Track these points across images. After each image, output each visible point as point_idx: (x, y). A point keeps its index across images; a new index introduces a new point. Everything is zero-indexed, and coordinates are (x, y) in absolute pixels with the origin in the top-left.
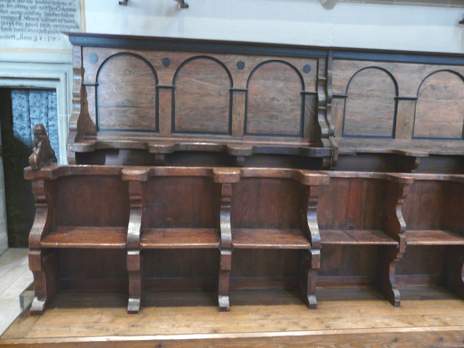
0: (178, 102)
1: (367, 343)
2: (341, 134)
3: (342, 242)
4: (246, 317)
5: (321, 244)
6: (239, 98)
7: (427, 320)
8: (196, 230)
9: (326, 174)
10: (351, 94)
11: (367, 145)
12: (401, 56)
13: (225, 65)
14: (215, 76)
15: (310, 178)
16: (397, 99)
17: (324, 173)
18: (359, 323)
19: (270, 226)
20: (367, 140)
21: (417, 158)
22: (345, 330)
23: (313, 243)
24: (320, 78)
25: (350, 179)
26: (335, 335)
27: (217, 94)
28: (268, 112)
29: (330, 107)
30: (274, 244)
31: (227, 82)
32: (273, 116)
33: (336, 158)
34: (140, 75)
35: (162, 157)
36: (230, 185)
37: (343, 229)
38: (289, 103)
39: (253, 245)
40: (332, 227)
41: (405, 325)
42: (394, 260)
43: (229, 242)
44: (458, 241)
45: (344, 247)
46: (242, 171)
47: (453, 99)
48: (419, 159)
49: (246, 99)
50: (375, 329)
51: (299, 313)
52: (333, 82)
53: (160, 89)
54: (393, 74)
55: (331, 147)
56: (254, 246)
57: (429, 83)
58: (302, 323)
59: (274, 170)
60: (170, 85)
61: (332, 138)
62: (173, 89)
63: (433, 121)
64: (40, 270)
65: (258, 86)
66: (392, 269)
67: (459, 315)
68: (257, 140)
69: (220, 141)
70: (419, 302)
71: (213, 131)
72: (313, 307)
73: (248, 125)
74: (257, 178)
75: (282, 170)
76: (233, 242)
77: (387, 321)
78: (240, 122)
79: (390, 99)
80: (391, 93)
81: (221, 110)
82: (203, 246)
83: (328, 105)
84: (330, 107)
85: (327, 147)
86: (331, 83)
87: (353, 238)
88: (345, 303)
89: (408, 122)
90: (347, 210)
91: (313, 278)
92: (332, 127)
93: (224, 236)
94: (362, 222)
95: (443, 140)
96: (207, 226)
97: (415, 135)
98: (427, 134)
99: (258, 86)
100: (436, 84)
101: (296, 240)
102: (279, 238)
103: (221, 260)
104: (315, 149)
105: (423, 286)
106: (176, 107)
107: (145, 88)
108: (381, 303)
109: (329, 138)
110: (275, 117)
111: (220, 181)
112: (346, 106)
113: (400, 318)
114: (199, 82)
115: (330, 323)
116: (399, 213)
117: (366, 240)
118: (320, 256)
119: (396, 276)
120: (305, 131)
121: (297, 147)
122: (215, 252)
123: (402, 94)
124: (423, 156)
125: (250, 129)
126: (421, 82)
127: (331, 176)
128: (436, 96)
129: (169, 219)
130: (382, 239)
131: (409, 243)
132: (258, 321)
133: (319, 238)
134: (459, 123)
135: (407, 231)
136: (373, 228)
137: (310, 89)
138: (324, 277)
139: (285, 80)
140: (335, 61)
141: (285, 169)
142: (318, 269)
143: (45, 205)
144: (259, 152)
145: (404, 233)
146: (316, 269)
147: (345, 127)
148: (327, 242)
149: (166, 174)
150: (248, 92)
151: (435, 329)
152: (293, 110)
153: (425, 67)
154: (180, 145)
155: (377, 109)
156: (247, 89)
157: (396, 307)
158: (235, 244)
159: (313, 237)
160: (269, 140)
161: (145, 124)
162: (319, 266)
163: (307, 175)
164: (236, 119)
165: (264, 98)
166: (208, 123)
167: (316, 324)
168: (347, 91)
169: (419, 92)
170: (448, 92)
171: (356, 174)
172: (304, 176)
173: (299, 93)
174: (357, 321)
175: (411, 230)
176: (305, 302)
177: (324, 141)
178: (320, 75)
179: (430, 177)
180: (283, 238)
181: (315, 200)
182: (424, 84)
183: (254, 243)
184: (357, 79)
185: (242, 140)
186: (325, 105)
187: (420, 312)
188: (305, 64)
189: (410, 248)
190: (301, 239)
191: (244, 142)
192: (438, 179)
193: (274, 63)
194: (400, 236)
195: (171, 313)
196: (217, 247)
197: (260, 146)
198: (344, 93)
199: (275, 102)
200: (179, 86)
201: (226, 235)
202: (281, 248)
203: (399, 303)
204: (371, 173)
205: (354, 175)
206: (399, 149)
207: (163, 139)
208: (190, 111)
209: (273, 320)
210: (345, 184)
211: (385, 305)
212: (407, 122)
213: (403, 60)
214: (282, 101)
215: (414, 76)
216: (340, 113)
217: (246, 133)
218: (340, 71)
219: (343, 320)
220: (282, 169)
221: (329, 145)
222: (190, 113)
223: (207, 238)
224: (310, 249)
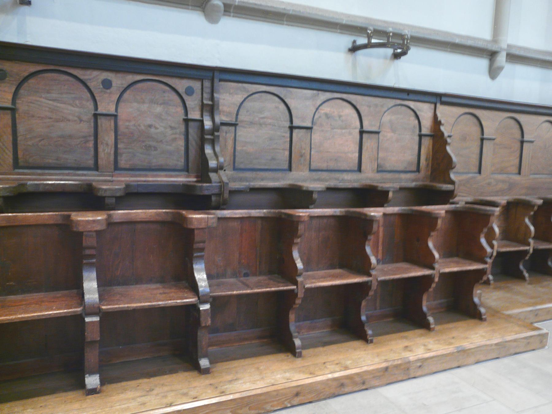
0: (21, 129)
1: (267, 403)
3: (235, 292)
4: (122, 396)
5: (211, 297)
6: (105, 124)
7: (328, 367)
8: (52, 294)
9: (214, 214)
10: (242, 121)
11: (262, 180)
12: (293, 81)
13: (86, 82)
14: (73, 96)
16: (292, 128)
17: (211, 213)
18: (258, 382)
19: (150, 281)
21: (314, 193)
22: (242, 393)
24: (205, 102)
25: (241, 219)
26: (231, 400)
27: (76, 118)
28: (143, 142)
29: (218, 136)
30: (154, 302)
32: (150, 146)
33: (226, 195)
36: (94, 234)
37: (237, 277)
38: (169, 132)
39: (126, 306)
40: (224, 275)
41: (307, 376)
42: (292, 307)
43: (95, 306)
44: (355, 278)
45: (239, 296)
46: (110, 216)
49: (115, 126)
50: (274, 386)
51: (189, 382)
52: (220, 108)
54: (286, 100)
55: (220, 182)
56: (128, 307)
57: (323, 112)
58: (193, 393)
59: (151, 212)
60: (9, 105)
61: (221, 172)
65: (130, 110)
66: (292, 317)
67: (359, 356)
68: (132, 177)
69: (83, 178)
70: (321, 349)
72: (206, 372)
73: (119, 158)
74: (131, 223)
75: (161, 212)
76: (101, 305)
77: (287, 375)
78: (109, 154)
79: (284, 127)
81: (83, 139)
83: (216, 134)
84: (218, 136)
85: (215, 182)
86: (218, 108)
87: (248, 286)
88: (242, 362)
89: (304, 153)
90: (240, 254)
91: (203, 337)
92: (221, 159)
93: (88, 299)
94: (258, 267)
97: (312, 167)
98: (324, 166)
99: (130, 110)
101: (181, 294)
102: (160, 294)
103: (86, 329)
105: (325, 330)
108: (282, 356)
109: (218, 173)
110: (153, 149)
111: (81, 229)
112: (237, 135)
113: (301, 370)
114: (50, 102)
115: (226, 387)
116: (296, 254)
117: (261, 287)
118: (210, 311)
119: (298, 324)
121: (181, 184)
122: (78, 319)
123: (296, 123)
124: (320, 189)
125: (122, 163)
126: (316, 109)
127: (220, 216)
128: (331, 125)
130: (279, 284)
131: (379, 279)
132: (139, 400)
133: (208, 290)
135: (304, 273)
136: (270, 272)
137: (195, 115)
138: (218, 334)
139: (165, 103)
140: (222, 83)
141: (164, 211)
142: (209, 326)
144: (136, 191)
145: (301, 276)
146: (206, 327)
147: (237, 159)
148: (217, 294)
150: (119, 118)
151: (336, 375)
152: (175, 140)
153: (319, 94)
154: (27, 184)
155: (271, 139)
156: (116, 113)
157: (298, 357)
158: (104, 307)
159: (201, 289)
160: (146, 176)
162: (209, 322)
163: (190, 216)
164: (104, 150)
165: (139, 125)
167: (209, 391)
168: (237, 118)
170: (342, 121)
171: (248, 213)
172: (187, 218)
173: (181, 119)
174: (255, 381)
175: (311, 271)
176: (196, 367)
177: (213, 176)
179: (326, 212)
180: (165, 293)
181: (201, 245)
182: (319, 112)
183: (127, 303)
185: (112, 177)
186: (212, 134)
187: (321, 359)
189: (443, 275)
190: (187, 293)
191: (114, 179)
192: (335, 214)
193: (149, 83)
195: (16, 410)
196: (79, 313)
197: (136, 183)
198: (234, 120)
199: (153, 130)
200: (22, 106)
201: (91, 296)
202: (162, 306)
204: (265, 211)
206: (296, 183)
208: (40, 141)
209: (157, 395)
210: (236, 224)
211: (286, 358)
214: (161, 129)
215: (308, 103)
217: (117, 168)
218: (228, 94)
219: (240, 382)
220: (161, 211)
221: (218, 180)
222: (40, 144)
223: (66, 302)
224: (197, 303)
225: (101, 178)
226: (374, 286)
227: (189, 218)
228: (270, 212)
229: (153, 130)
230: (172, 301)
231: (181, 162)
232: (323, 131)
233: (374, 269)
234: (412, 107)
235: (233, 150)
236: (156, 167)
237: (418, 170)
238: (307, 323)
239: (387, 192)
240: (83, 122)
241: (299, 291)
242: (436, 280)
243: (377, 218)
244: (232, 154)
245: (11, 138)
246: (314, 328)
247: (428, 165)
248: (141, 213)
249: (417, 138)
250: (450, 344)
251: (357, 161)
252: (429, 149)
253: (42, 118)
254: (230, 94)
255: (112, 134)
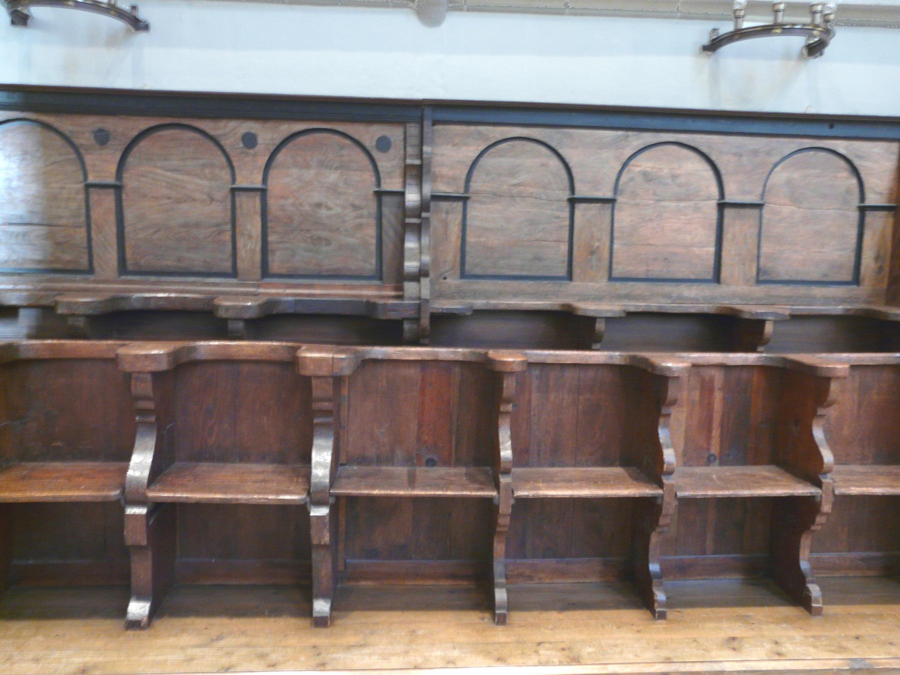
2: (458, 272)
6: (250, 205)
10: (477, 193)
14: (201, 162)
15: (308, 361)
16: (573, 202)
19: (262, 458)
20: (514, 284)
21: (598, 320)
23: (312, 492)
25: (422, 364)
27: (205, 197)
28: (308, 231)
29: (427, 219)
31: (226, 175)
32: (319, 238)
34: (53, 163)
35: (81, 323)
38: (350, 214)
43: (140, 490)
47: (690, 200)
48: (603, 320)
53: (91, 190)
54: (561, 151)
56: (187, 498)
57: (638, 169)
59: (263, 346)
62: (118, 189)
63: (652, 245)
64: (145, 543)
71: (202, 270)
72: (321, 623)
73: (270, 258)
78: (253, 251)
79: (559, 200)
80: (560, 190)
81: (215, 229)
82: (85, 496)
83: (424, 215)
85: (411, 298)
86: (429, 171)
89: (598, 247)
90: (420, 425)
94: (454, 451)
95: (675, 284)
96: (280, 459)
97: (615, 274)
98: (640, 270)
99: (288, 180)
100: (654, 170)
104: (385, 304)
106: (126, 224)
107: (63, 188)
112: (468, 216)
114: (169, 174)
116: (818, 434)
118: (327, 520)
120: (385, 269)
121: (364, 300)
123: (582, 191)
124: (609, 315)
125: (276, 263)
128: (655, 194)
129: (59, 444)
134: (706, 249)
135: (514, 470)
137: (392, 184)
139: (342, 167)
140: (438, 127)
143: (330, 420)
144: (291, 311)
149: (46, 355)
150: (269, 194)
152: (360, 227)
154: (131, 298)
155: (532, 222)
161: (67, 257)
164: (245, 246)
165: (301, 204)
166: (190, 255)
169: (620, 187)
170: (680, 185)
176: (307, 612)
178: (411, 155)
179: (591, 357)
184: (486, 161)
186: (419, 216)
188: (379, 136)
189: (523, 504)
193: (318, 135)
194: (823, 480)
196: (114, 499)
198: (462, 190)
199: (323, 212)
200: (130, 181)
203: (504, 616)
205: (428, 353)
207: (101, 286)
208: (156, 232)
212: (595, 247)
213: (515, 122)
214: (337, 210)
215: (605, 154)
216: (455, 230)
217: (265, 272)
222: (155, 237)
225: (241, 289)
226: (670, 507)
227: (301, 357)
228: (474, 353)
229: (323, 212)
230: (261, 496)
231: (371, 264)
232: (637, 205)
233: (670, 473)
234: (842, 151)
235: (459, 242)
236: (330, 273)
237: (856, 280)
238: (551, 562)
239: (762, 323)
240: (214, 203)
241: (501, 501)
242: (826, 508)
243: (674, 372)
244: (458, 250)
245: (114, 229)
246: (563, 574)
247: (881, 269)
248: (247, 346)
249: (854, 215)
250: (842, 649)
251: (711, 262)
252: (883, 236)
253: (157, 198)
254: (454, 145)
255: (258, 219)
